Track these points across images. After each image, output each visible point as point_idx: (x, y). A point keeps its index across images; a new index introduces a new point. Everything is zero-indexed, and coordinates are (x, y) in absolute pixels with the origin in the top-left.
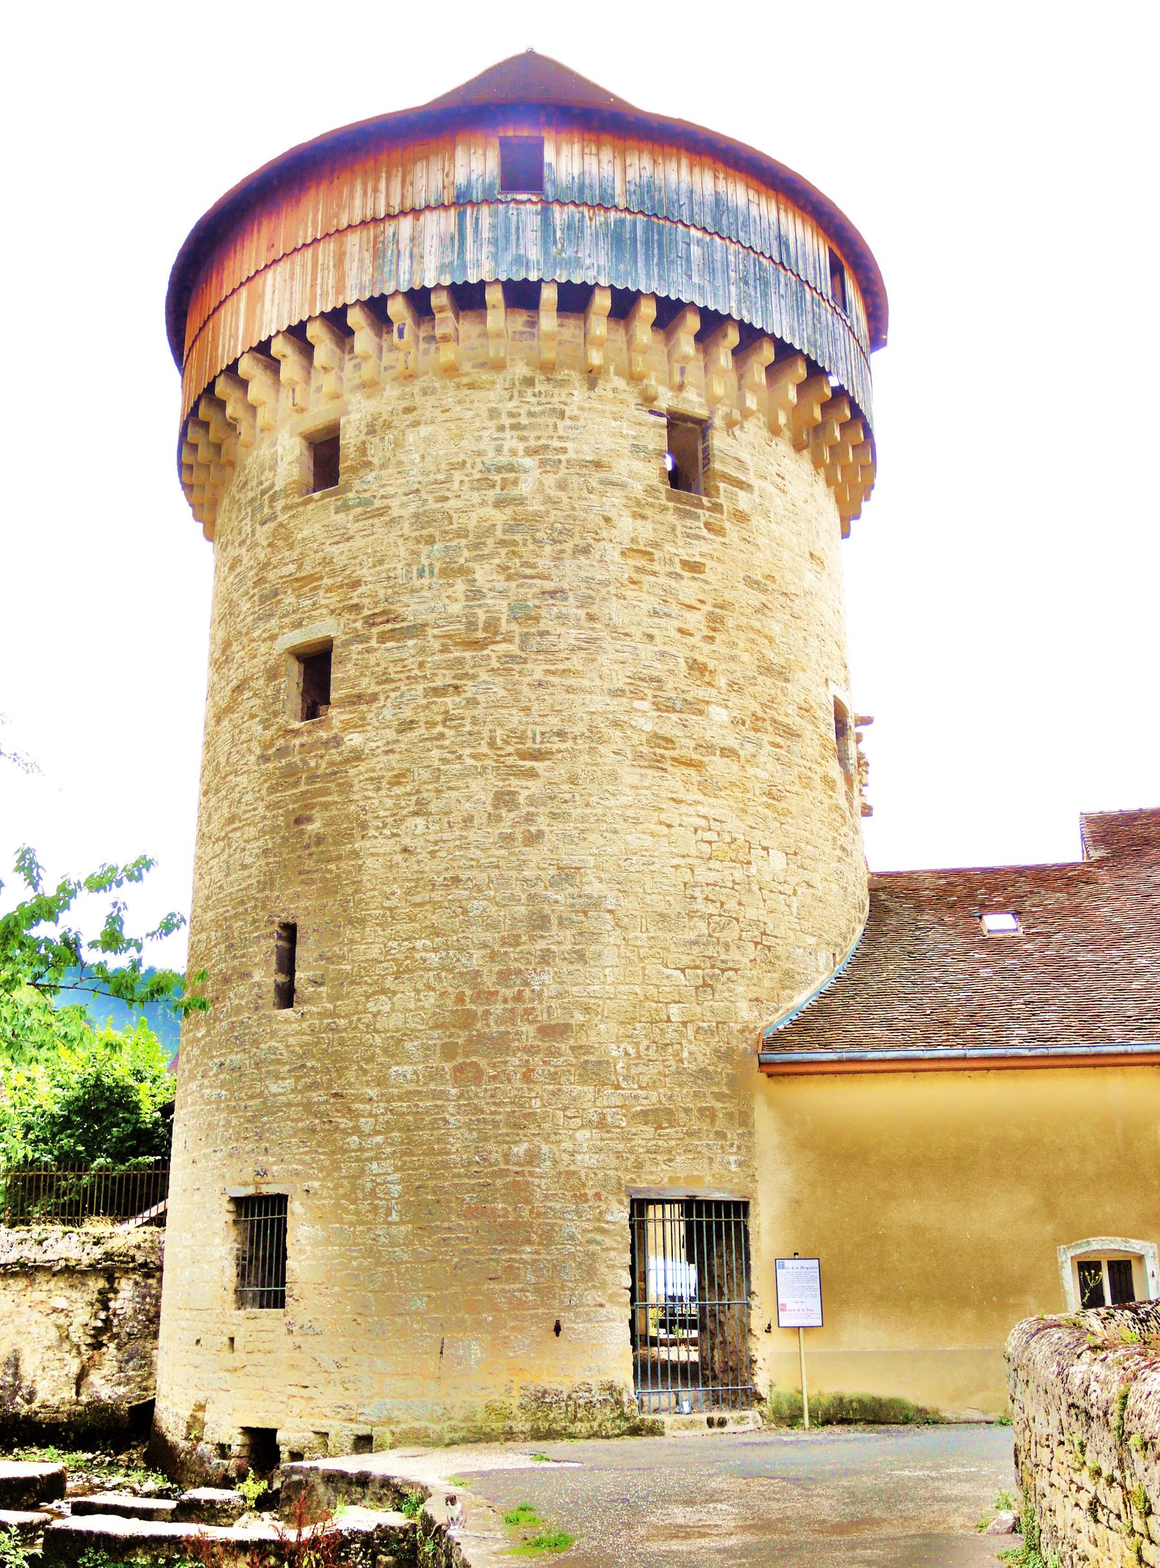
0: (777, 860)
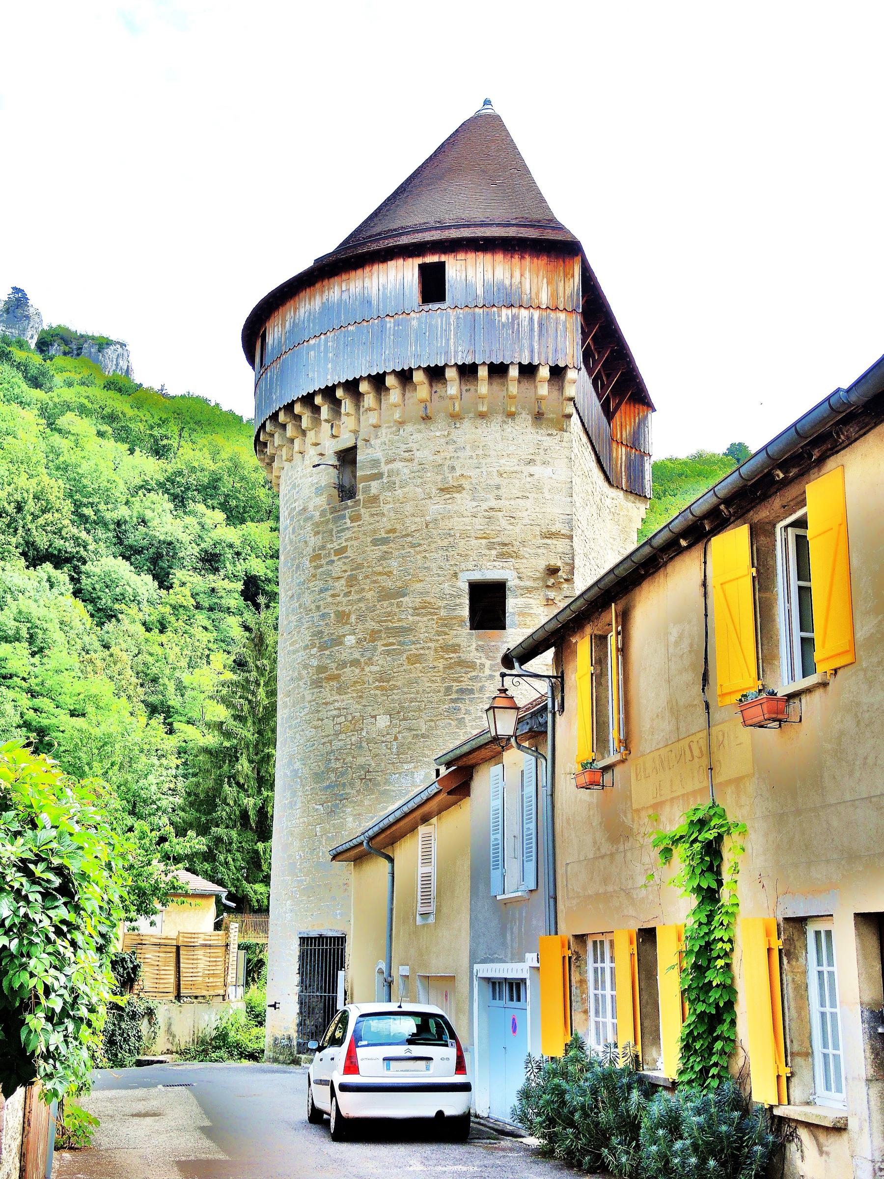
0: (383, 722)
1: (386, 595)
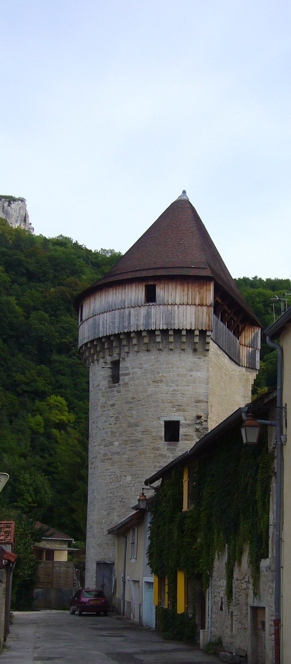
0: (129, 478)
1: (130, 425)
